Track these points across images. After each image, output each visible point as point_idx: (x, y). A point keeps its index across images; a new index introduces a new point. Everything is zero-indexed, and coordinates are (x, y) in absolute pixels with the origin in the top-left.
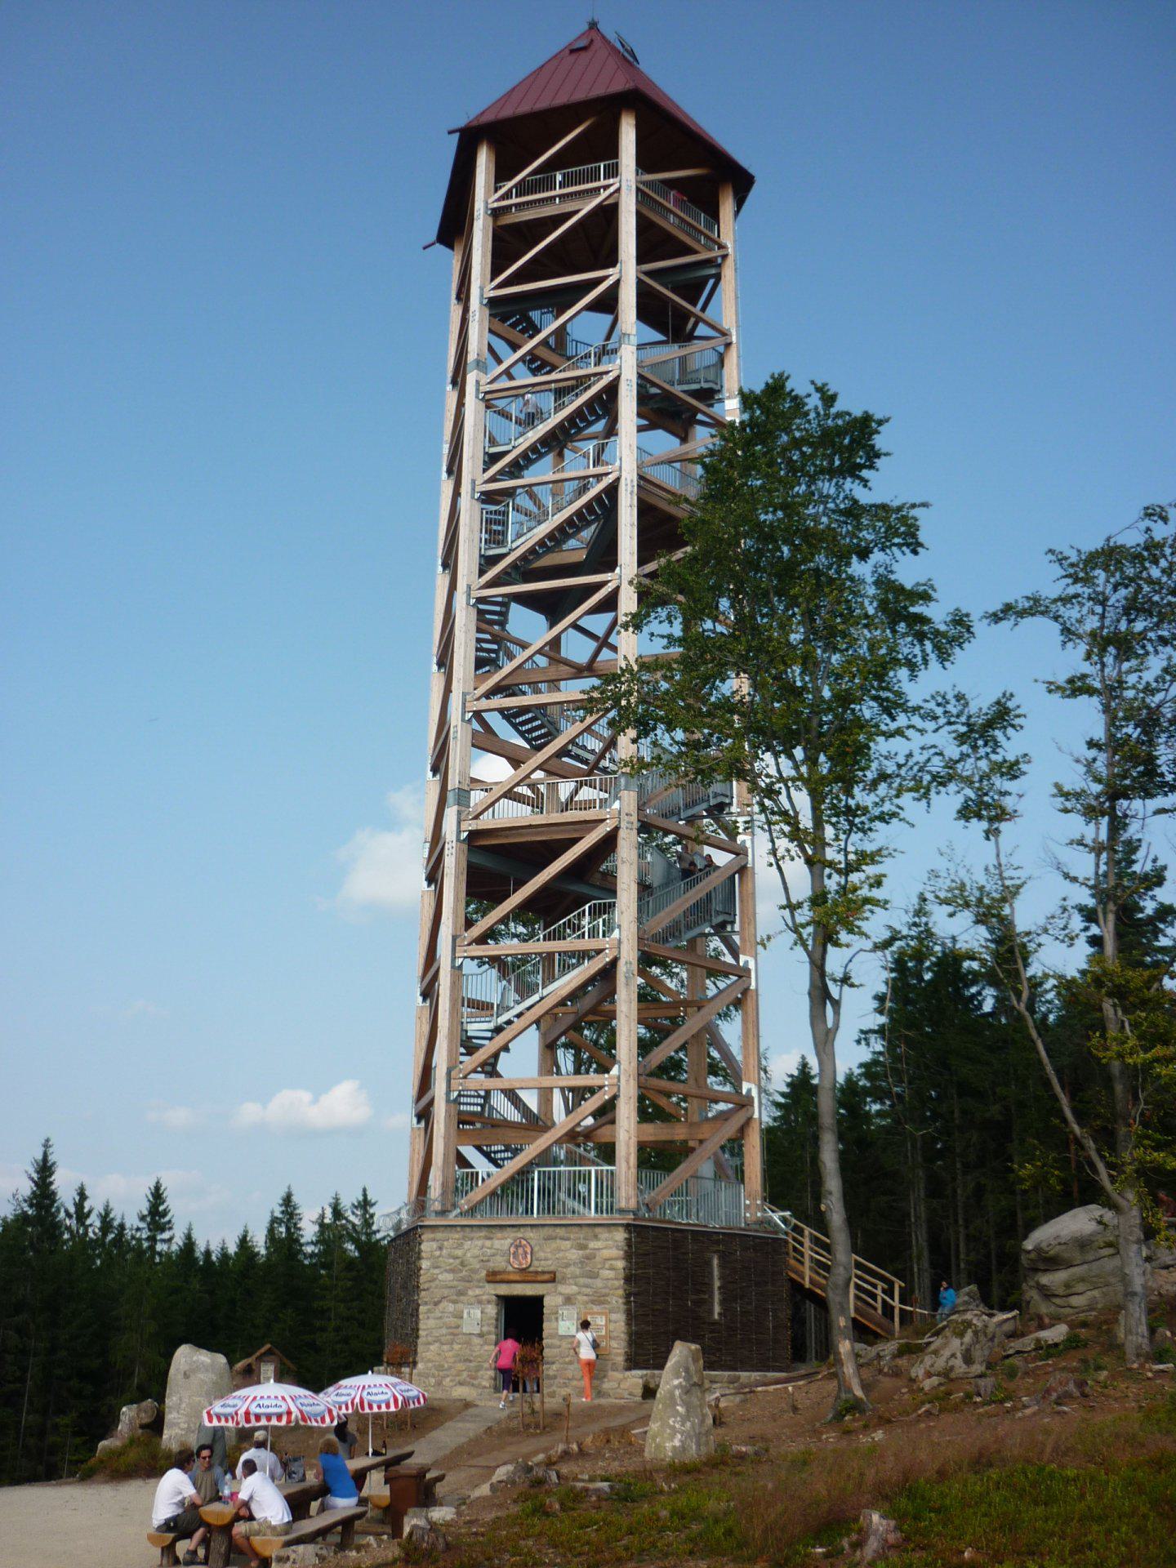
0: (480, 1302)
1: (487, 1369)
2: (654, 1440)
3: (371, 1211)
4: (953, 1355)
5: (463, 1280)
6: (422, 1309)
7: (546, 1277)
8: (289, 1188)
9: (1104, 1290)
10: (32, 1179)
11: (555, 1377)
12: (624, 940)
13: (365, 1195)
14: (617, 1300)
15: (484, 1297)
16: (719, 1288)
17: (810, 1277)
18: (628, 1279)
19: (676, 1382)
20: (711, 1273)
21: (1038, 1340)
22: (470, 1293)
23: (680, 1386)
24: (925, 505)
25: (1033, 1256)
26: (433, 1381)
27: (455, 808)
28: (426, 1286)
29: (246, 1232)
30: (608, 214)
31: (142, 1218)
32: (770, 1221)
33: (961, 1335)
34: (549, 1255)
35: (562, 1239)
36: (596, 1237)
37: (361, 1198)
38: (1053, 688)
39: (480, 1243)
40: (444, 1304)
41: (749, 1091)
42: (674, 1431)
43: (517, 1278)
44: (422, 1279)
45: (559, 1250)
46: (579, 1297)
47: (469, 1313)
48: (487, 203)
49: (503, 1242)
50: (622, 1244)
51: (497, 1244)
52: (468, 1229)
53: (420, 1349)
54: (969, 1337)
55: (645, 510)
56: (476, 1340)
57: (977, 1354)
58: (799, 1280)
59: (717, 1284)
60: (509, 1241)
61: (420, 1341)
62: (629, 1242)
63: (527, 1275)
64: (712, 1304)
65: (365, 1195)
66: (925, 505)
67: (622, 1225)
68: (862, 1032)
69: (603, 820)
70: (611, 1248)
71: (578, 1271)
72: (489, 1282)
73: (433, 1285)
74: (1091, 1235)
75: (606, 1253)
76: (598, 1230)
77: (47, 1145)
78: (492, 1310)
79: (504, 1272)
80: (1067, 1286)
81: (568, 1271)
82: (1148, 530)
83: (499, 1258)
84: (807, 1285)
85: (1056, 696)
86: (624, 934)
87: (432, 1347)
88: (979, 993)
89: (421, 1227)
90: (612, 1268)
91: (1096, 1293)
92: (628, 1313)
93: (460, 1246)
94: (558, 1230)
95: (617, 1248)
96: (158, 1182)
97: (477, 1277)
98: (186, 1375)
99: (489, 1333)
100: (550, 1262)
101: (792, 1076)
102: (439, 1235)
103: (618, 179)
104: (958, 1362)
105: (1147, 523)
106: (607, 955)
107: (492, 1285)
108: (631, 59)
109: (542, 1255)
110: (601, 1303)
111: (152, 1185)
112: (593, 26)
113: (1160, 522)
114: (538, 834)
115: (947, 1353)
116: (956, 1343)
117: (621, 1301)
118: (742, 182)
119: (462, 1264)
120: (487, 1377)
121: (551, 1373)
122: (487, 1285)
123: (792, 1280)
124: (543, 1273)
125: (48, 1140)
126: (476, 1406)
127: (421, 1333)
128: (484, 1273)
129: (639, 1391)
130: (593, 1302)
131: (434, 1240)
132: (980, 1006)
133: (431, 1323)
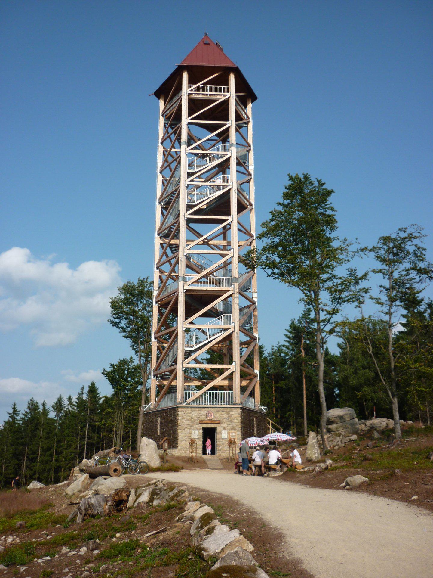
0: (197, 429)
4: (338, 441)
5: (192, 423)
6: (179, 431)
7: (217, 422)
11: (221, 450)
14: (239, 428)
18: (241, 423)
19: (314, 441)
21: (350, 439)
22: (194, 426)
23: (315, 442)
26: (183, 452)
28: (180, 424)
30: (226, 103)
33: (339, 436)
36: (232, 411)
39: (197, 412)
40: (186, 430)
44: (179, 422)
45: (221, 414)
49: (204, 412)
50: (240, 413)
51: (202, 412)
53: (179, 443)
54: (341, 437)
57: (343, 441)
60: (206, 412)
61: (179, 440)
63: (211, 422)
67: (240, 408)
69: (229, 291)
70: (236, 414)
71: (227, 420)
75: (235, 415)
78: (201, 431)
79: (205, 420)
80: (337, 428)
81: (224, 420)
82: (398, 233)
87: (183, 442)
89: (178, 407)
90: (237, 420)
92: (242, 432)
95: (239, 414)
98: (147, 445)
99: (201, 438)
104: (340, 443)
105: (399, 232)
109: (216, 416)
110: (234, 429)
113: (403, 232)
115: (336, 441)
116: (338, 439)
117: (240, 429)
119: (192, 418)
121: (220, 449)
127: (179, 438)
128: (199, 421)
130: (231, 429)
133: (182, 435)
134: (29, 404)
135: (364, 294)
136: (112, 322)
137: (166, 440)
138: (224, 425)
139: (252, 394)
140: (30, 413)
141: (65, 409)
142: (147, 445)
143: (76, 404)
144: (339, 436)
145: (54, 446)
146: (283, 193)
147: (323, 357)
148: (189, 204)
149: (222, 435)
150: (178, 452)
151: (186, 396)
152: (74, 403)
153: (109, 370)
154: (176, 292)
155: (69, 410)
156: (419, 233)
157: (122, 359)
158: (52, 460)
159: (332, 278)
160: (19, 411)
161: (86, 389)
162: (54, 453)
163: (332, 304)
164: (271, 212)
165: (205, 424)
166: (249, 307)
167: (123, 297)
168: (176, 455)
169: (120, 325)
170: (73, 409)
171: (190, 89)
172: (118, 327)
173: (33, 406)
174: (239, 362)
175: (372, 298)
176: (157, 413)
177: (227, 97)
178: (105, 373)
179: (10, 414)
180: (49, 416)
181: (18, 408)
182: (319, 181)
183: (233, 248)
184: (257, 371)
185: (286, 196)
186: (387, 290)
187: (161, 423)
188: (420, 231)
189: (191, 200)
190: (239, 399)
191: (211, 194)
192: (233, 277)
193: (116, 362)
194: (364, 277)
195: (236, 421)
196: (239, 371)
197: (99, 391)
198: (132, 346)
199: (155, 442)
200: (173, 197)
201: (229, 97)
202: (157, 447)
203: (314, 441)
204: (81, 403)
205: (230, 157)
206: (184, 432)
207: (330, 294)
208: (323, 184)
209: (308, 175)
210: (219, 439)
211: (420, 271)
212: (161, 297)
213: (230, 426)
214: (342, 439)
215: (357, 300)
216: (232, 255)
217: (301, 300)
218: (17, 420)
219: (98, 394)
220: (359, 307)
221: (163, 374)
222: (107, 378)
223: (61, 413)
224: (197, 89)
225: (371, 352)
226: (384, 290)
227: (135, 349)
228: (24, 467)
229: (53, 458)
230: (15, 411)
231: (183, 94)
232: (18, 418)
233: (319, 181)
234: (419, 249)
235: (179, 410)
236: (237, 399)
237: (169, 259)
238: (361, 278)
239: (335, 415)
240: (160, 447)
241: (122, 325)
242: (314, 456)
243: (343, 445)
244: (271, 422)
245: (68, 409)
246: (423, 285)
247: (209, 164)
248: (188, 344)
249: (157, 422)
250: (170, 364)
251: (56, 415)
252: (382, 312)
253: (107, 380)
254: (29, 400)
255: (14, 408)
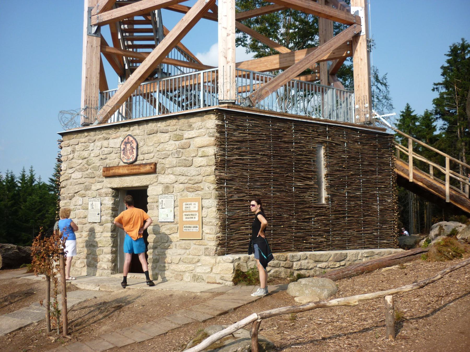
1: (106, 253)
7: (148, 168)
15: (103, 191)
16: (327, 175)
17: (414, 173)
20: (319, 163)
22: (94, 187)
34: (151, 149)
43: (125, 171)
47: (92, 205)
50: (213, 130)
58: (405, 176)
59: (324, 172)
62: (220, 129)
64: (319, 189)
68: (435, 84)
72: (107, 177)
73: (69, 182)
75: (199, 142)
81: (167, 161)
83: (113, 155)
84: (411, 179)
92: (220, 198)
99: (107, 222)
100: (152, 155)
101: (403, 112)
107: (108, 180)
120: (105, 260)
122: (104, 179)
123: (399, 177)
124: (146, 164)
126: (77, 289)
129: (230, 276)
130: (187, 189)
146: (454, 45)
149: (161, 210)
164: (433, 90)
165: (117, 180)
213: (182, 179)
244: (448, 158)
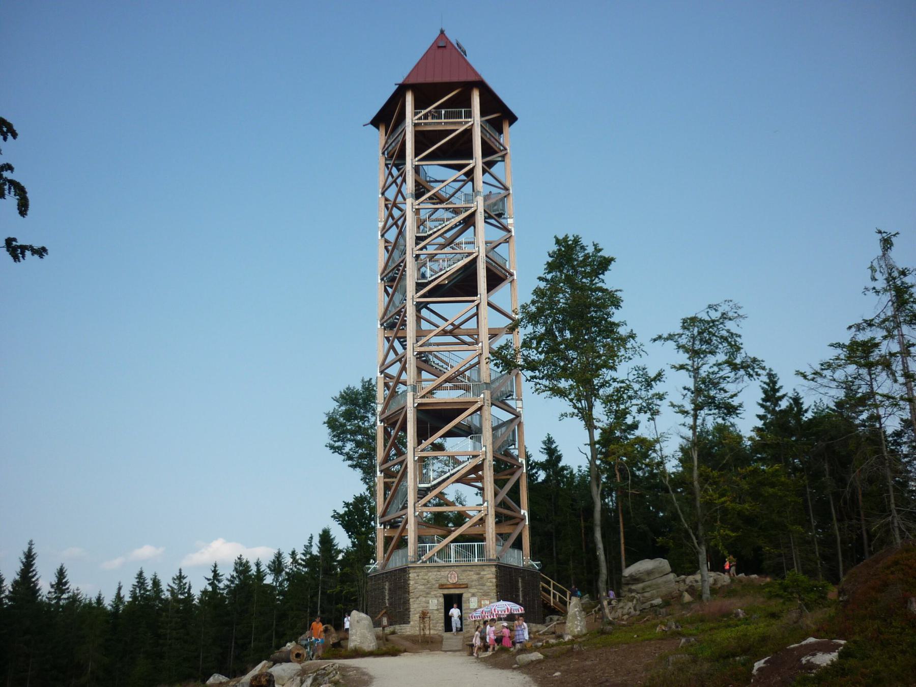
0: (436, 597)
2: (569, 628)
3: (184, 581)
4: (630, 608)
5: (428, 588)
6: (411, 600)
7: (464, 586)
8: (141, 569)
9: (658, 590)
10: (22, 562)
11: (469, 625)
12: (488, 451)
13: (180, 573)
18: (497, 586)
19: (576, 610)
21: (652, 604)
22: (432, 593)
23: (578, 611)
24: (620, 291)
25: (628, 578)
27: (412, 393)
29: (100, 595)
30: (468, 133)
31: (52, 586)
32: (532, 565)
33: (632, 601)
35: (470, 571)
36: (484, 570)
37: (178, 574)
38: (674, 367)
39: (435, 573)
41: (524, 514)
42: (577, 626)
44: (411, 588)
45: (469, 575)
46: (478, 594)
48: (412, 120)
50: (494, 572)
51: (442, 573)
52: (429, 568)
54: (635, 602)
55: (489, 271)
56: (435, 612)
57: (637, 607)
61: (411, 613)
63: (456, 586)
65: (180, 573)
66: (620, 291)
67: (495, 565)
70: (490, 574)
71: (477, 584)
74: (652, 569)
75: (488, 576)
76: (484, 567)
77: (31, 543)
78: (442, 600)
79: (446, 585)
80: (643, 589)
81: (473, 583)
82: (708, 312)
85: (673, 370)
86: (488, 449)
88: (536, 473)
90: (491, 582)
91: (654, 591)
93: (426, 575)
94: (468, 567)
95: (493, 574)
96: (62, 566)
97: (434, 587)
99: (441, 609)
102: (417, 571)
103: (472, 119)
104: (632, 610)
105: (708, 310)
106: (480, 458)
108: (462, 54)
109: (461, 577)
111: (59, 567)
112: (442, 32)
113: (714, 311)
114: (447, 406)
115: (627, 607)
116: (630, 604)
117: (495, 594)
118: (512, 119)
119: (428, 582)
125: (31, 541)
127: (411, 610)
130: (483, 595)
131: (415, 572)
132: (537, 479)
133: (415, 606)
134: (236, 564)
135: (659, 402)
136: (332, 447)
137: (385, 613)
138: (473, 591)
139: (518, 544)
140: (238, 577)
141: (287, 570)
142: (358, 622)
143: (303, 563)
144: (632, 601)
145: (272, 625)
147: (599, 492)
148: (420, 281)
150: (411, 628)
151: (421, 552)
152: (300, 561)
153: (342, 511)
154: (404, 408)
155: (293, 571)
156: (736, 313)
157: (358, 495)
158: (271, 646)
159: (611, 382)
160: (222, 575)
161: (316, 540)
162: (274, 636)
163: (608, 420)
166: (512, 421)
167: (343, 408)
168: (408, 633)
169: (344, 449)
170: (298, 569)
171: (417, 117)
172: (341, 454)
173: (242, 567)
174: (493, 502)
175: (673, 405)
176: (385, 576)
177: (470, 124)
178: (337, 516)
179: (209, 580)
180: (265, 582)
181: (220, 571)
182: (595, 245)
183: (482, 342)
184: (524, 512)
185: (550, 267)
186: (692, 393)
187: (390, 590)
188: (735, 311)
189: (423, 276)
190: (494, 553)
191: (450, 266)
192: (483, 382)
193: (351, 500)
194: (659, 377)
195: (488, 584)
196: (493, 513)
197: (335, 542)
198: (364, 479)
199: (369, 617)
200: (397, 274)
201: (472, 125)
202: (371, 624)
203: (576, 610)
204: (311, 561)
205: (475, 211)
206: (418, 602)
207: (604, 406)
208: (600, 250)
209: (580, 237)
210: (467, 609)
211: (735, 367)
212: (387, 413)
213: (481, 591)
214: (636, 604)
215: (650, 410)
216: (480, 352)
217: (562, 415)
218: (220, 589)
219: (335, 546)
220: (653, 419)
221: (392, 521)
222: (339, 524)
223: (281, 575)
224: (426, 116)
225: (667, 482)
226: (689, 393)
227: (367, 483)
228: (232, 657)
229: (272, 643)
230: (216, 575)
231: (407, 124)
232: (221, 585)
233: (595, 245)
234: (732, 334)
235: (410, 571)
236: (491, 553)
237: (399, 357)
238: (655, 379)
239: (641, 569)
240: (377, 624)
241: (347, 450)
242: (576, 630)
243: (638, 613)
244: (552, 582)
245: (291, 569)
246: (741, 386)
247: (446, 223)
248: (424, 478)
249: (384, 588)
250: (401, 507)
251: (273, 580)
252: (684, 425)
253: (340, 526)
254: (237, 559)
255: (215, 571)
